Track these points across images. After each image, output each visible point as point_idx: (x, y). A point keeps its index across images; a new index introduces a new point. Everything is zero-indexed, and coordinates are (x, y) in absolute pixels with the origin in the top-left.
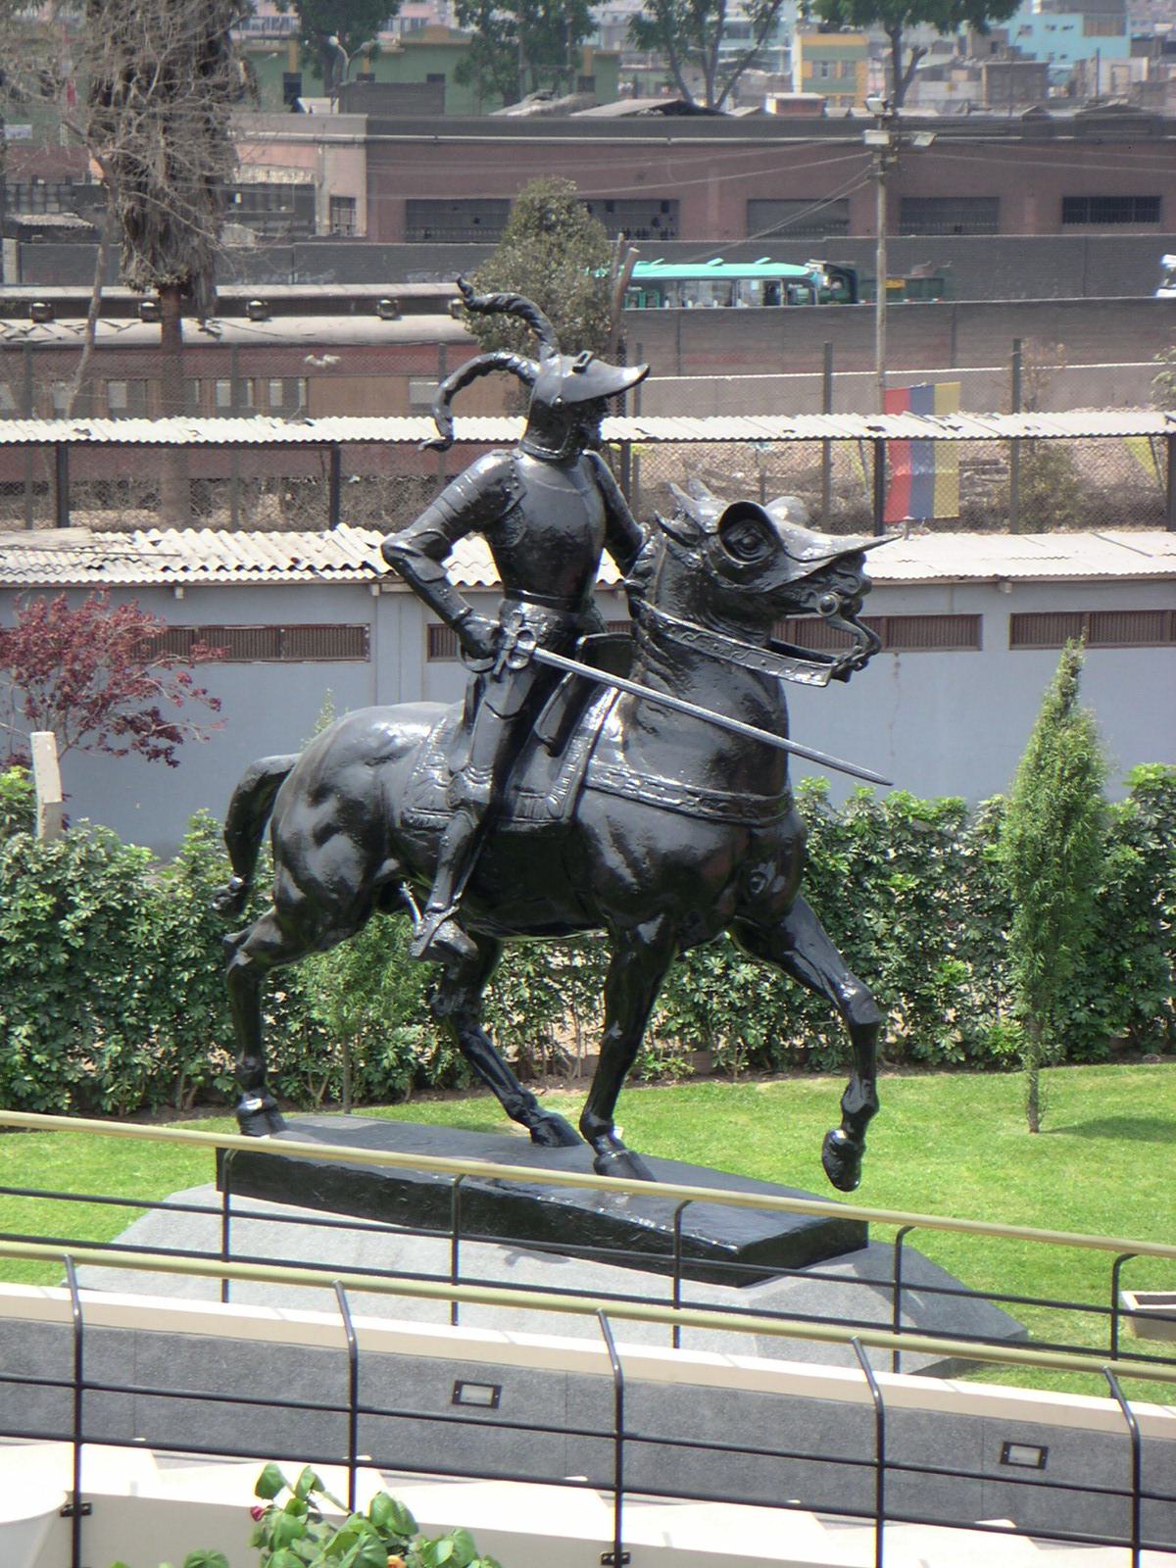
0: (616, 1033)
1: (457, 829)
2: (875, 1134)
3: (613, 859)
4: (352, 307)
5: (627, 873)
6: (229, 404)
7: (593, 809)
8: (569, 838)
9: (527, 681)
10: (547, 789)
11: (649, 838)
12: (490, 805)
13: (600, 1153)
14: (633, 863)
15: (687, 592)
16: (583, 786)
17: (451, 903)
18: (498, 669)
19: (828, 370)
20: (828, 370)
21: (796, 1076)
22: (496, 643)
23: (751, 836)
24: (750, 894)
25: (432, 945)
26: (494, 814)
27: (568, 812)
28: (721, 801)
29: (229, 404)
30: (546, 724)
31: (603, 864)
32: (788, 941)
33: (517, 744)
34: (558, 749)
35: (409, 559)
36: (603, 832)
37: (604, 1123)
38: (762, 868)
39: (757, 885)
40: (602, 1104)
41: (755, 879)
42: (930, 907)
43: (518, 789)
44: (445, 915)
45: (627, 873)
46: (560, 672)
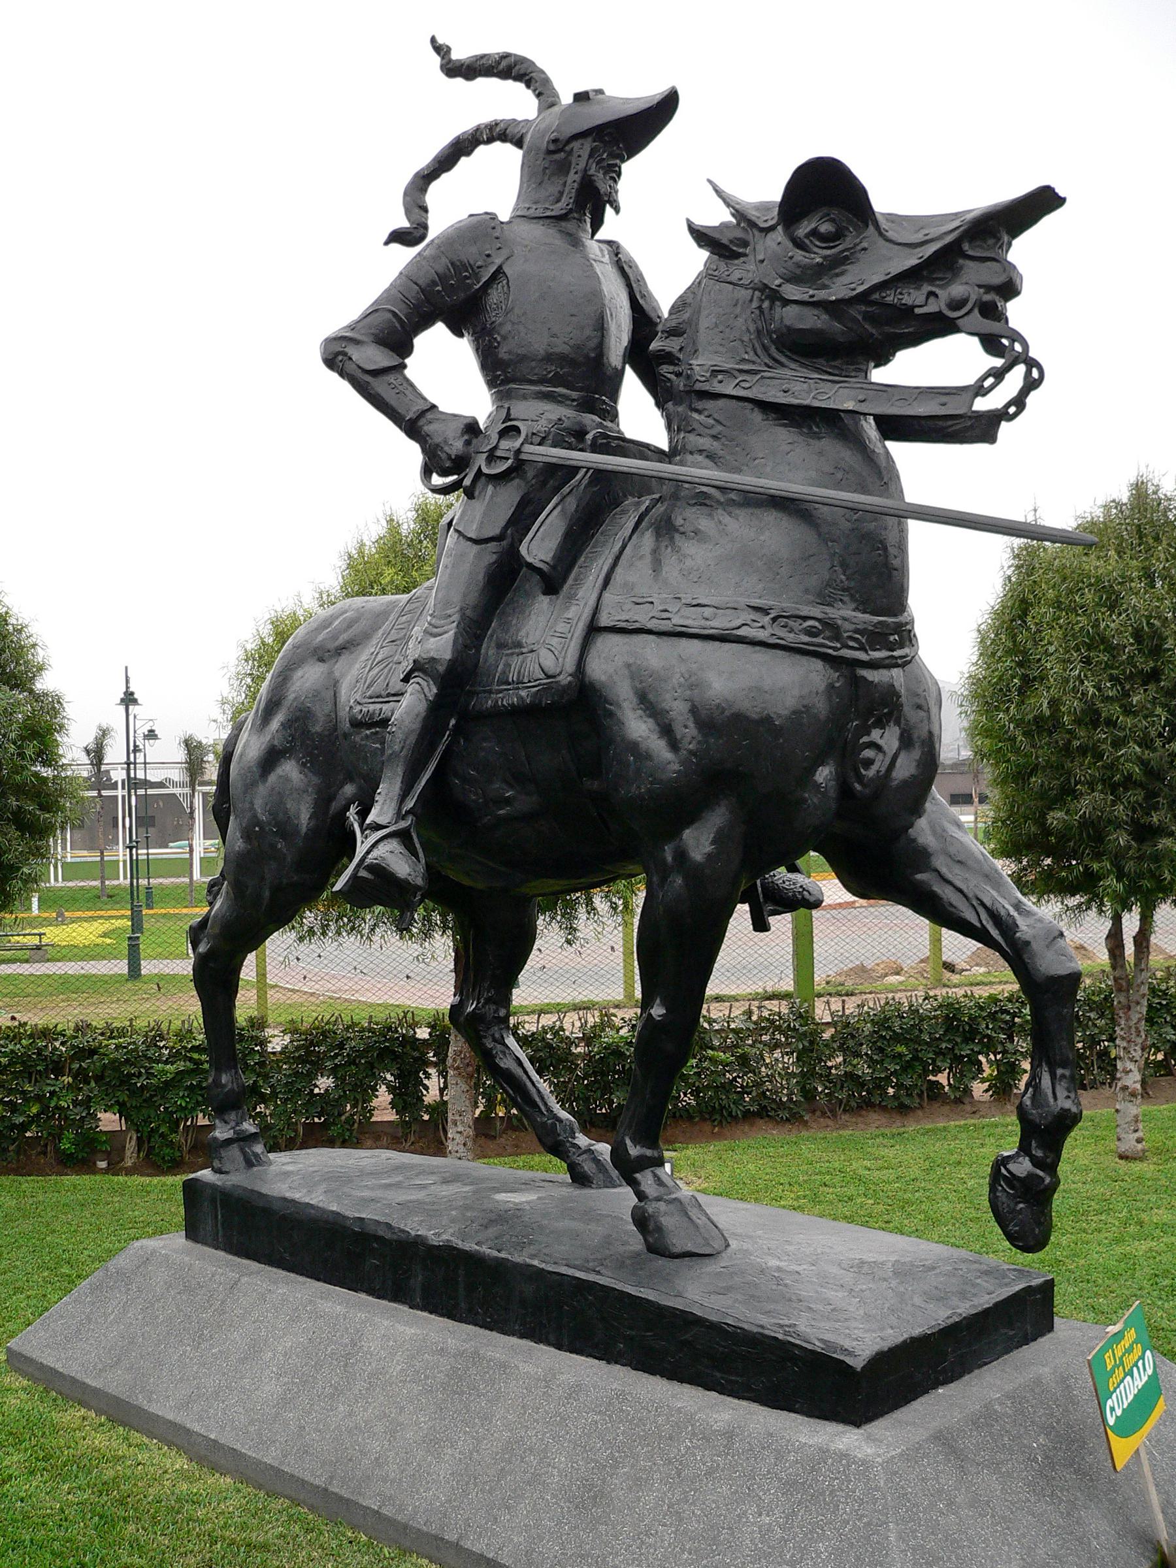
0: (657, 1011)
1: (409, 707)
3: (638, 727)
4: (418, 1280)
5: (658, 747)
6: (966, 754)
7: (609, 663)
9: (506, 499)
11: (691, 687)
12: (452, 663)
13: (641, 1196)
14: (667, 731)
16: (594, 630)
17: (400, 816)
18: (467, 482)
23: (856, 682)
24: (860, 778)
25: (363, 873)
26: (455, 685)
27: (570, 665)
29: (966, 754)
30: (539, 547)
31: (623, 739)
33: (505, 582)
36: (623, 693)
38: (875, 735)
39: (869, 763)
41: (868, 753)
43: (501, 646)
45: (658, 747)
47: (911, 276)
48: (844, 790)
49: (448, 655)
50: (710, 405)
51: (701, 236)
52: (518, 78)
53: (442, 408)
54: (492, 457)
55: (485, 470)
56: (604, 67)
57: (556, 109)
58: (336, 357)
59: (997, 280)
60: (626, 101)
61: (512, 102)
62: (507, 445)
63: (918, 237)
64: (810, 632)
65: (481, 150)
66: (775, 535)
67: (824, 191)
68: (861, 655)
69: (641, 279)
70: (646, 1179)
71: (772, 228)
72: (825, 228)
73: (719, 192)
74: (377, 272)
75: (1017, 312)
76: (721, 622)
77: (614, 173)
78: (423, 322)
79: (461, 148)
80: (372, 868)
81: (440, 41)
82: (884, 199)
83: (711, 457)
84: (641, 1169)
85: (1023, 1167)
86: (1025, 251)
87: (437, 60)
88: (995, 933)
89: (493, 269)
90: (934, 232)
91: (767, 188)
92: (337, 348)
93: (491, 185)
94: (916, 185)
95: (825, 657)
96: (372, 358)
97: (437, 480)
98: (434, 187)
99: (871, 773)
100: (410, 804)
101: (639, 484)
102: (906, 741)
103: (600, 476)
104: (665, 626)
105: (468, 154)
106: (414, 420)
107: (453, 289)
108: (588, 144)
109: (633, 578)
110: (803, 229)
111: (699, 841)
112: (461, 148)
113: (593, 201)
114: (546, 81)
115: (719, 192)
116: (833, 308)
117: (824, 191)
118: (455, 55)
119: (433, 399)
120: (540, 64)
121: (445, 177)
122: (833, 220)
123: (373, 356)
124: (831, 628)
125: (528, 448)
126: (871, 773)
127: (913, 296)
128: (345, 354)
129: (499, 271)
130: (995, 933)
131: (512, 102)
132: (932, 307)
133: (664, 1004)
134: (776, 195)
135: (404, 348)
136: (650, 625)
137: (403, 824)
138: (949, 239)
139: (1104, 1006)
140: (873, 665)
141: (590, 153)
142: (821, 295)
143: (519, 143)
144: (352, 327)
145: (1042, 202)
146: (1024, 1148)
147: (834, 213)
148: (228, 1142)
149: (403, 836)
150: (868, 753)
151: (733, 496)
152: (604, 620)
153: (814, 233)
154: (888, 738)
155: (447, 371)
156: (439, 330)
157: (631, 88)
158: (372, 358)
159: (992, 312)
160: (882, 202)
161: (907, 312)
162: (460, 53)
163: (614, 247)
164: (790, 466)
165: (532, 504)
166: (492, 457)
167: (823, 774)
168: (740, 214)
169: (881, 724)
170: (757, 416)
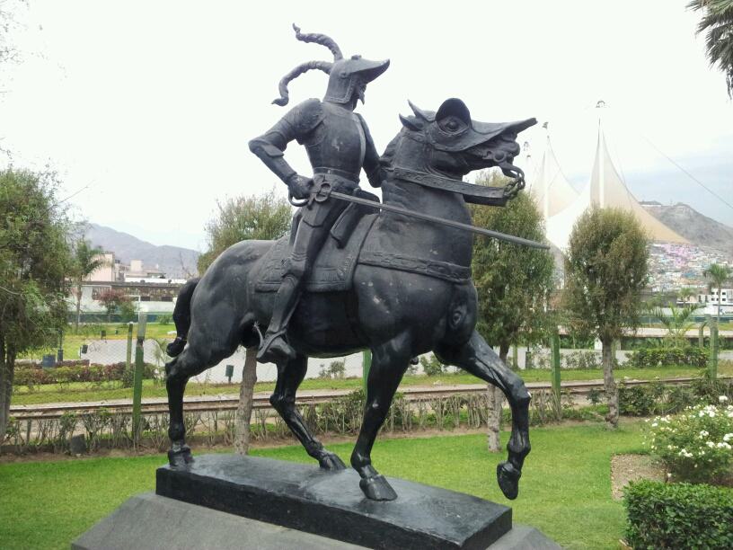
2: (529, 465)
8: (347, 297)
9: (325, 211)
10: (335, 267)
14: (388, 303)
15: (417, 155)
16: (358, 263)
17: (280, 329)
18: (310, 203)
19: (137, 405)
20: (137, 405)
21: (251, 487)
22: (310, 189)
24: (453, 322)
25: (269, 351)
26: (305, 278)
27: (349, 276)
28: (439, 266)
30: (337, 230)
32: (471, 352)
34: (341, 244)
35: (263, 146)
37: (366, 459)
38: (459, 309)
39: (456, 318)
40: (365, 446)
41: (457, 315)
42: (504, 351)
44: (277, 335)
46: (347, 203)
47: (484, 145)
48: (448, 328)
49: (303, 270)
50: (405, 185)
51: (404, 121)
52: (326, 45)
53: (298, 174)
54: (319, 194)
55: (317, 200)
56: (359, 46)
57: (341, 61)
58: (256, 147)
59: (513, 150)
60: (374, 63)
61: (323, 54)
62: (325, 190)
63: (485, 131)
64: (442, 271)
65: (310, 71)
66: (429, 235)
67: (454, 111)
68: (457, 280)
69: (368, 130)
70: (366, 471)
71: (432, 122)
72: (452, 124)
73: (411, 105)
74: (270, 119)
75: (517, 162)
76: (410, 265)
77: (364, 88)
78: (290, 139)
79: (302, 69)
80: (273, 350)
81: (297, 25)
82: (475, 116)
83: (405, 204)
84: (364, 466)
85: (509, 467)
86: (521, 138)
87: (294, 33)
88: (499, 381)
89: (319, 122)
90: (496, 129)
91: (432, 106)
92: (256, 144)
93: (314, 88)
94: (487, 113)
95: (445, 281)
96: (269, 150)
97: (294, 200)
98: (290, 83)
99: (457, 322)
100: (285, 324)
101: (370, 210)
102: (469, 311)
103: (358, 206)
104: (387, 265)
105: (305, 72)
106: (288, 177)
107: (304, 128)
108: (356, 77)
109: (371, 242)
110: (445, 122)
111: (397, 344)
112: (302, 69)
113: (356, 96)
114: (338, 48)
115: (411, 105)
116: (451, 153)
117: (454, 111)
118: (302, 32)
119: (295, 169)
120: (335, 41)
121: (294, 79)
122: (455, 121)
123: (271, 150)
124: (447, 269)
125: (333, 193)
126: (457, 322)
127: (483, 153)
128: (260, 147)
129: (321, 123)
130: (499, 381)
131: (323, 54)
132: (489, 157)
133: (377, 403)
134: (436, 110)
135: (283, 147)
136: (382, 264)
137: (282, 332)
138: (497, 133)
139: (89, 442)
140: (460, 284)
141: (355, 81)
142: (450, 149)
143: (327, 71)
144: (262, 137)
145: (294, 25)
146: (510, 460)
147: (455, 118)
148: (178, 453)
149: (282, 336)
150: (457, 315)
151: (413, 219)
152: (362, 259)
153: (448, 125)
154: (463, 310)
155: (297, 157)
156: (295, 141)
157: (372, 57)
158: (269, 150)
159: (510, 160)
160: (473, 117)
161: (480, 158)
162: (304, 32)
163: (358, 115)
164: (434, 211)
165: (332, 216)
166: (319, 194)
167: (442, 322)
168: (418, 114)
169: (461, 304)
170: (422, 190)
